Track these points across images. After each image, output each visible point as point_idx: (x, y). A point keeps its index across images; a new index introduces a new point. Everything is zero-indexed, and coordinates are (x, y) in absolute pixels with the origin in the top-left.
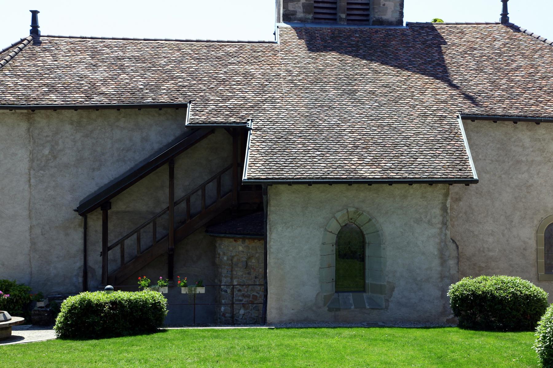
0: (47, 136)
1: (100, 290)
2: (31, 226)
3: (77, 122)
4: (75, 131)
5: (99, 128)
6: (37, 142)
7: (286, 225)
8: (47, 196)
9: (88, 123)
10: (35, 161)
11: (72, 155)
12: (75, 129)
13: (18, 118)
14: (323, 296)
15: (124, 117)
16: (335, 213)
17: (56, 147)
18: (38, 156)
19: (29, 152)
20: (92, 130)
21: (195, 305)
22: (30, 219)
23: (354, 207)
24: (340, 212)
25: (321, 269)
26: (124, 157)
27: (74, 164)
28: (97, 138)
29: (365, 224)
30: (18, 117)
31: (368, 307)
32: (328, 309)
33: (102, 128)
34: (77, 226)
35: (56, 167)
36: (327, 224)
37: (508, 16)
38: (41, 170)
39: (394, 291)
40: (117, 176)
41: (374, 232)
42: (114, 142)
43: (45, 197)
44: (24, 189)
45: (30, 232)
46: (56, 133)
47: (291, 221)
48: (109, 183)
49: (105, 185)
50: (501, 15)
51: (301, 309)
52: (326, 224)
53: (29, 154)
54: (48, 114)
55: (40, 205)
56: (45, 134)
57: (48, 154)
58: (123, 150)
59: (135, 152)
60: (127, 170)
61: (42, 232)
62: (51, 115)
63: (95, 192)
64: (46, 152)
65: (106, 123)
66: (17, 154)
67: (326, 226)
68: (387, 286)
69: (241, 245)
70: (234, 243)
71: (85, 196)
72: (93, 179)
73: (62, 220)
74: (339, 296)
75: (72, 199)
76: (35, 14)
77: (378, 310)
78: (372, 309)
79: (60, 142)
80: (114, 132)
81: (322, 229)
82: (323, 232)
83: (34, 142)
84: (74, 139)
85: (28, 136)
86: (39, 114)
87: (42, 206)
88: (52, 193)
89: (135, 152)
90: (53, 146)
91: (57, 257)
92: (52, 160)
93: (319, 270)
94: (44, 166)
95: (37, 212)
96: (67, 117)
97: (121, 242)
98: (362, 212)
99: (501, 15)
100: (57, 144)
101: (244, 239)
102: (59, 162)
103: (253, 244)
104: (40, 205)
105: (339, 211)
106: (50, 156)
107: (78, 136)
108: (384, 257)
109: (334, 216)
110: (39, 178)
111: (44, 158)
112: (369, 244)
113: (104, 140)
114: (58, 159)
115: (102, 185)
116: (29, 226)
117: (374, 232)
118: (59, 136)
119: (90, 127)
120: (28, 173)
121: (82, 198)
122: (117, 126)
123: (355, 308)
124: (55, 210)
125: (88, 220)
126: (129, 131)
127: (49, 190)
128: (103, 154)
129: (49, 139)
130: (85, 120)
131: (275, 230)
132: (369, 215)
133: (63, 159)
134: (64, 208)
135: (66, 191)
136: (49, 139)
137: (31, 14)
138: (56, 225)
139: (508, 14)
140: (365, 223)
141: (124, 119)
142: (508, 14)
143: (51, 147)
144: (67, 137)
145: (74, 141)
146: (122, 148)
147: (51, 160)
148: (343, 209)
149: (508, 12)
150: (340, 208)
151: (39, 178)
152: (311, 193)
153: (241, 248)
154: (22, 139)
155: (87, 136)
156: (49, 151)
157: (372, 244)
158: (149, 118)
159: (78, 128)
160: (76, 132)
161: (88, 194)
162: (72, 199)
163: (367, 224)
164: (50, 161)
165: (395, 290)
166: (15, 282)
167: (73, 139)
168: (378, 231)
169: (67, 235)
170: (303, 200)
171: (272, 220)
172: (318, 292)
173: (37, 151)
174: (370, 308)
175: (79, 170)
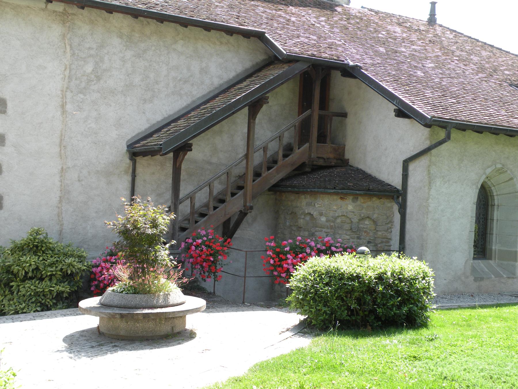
0: (90, 48)
2: (62, 168)
3: (128, 36)
4: (125, 48)
5: (153, 48)
6: (77, 54)
7: (444, 180)
8: (86, 130)
9: (141, 39)
10: (74, 80)
11: (120, 79)
12: (125, 45)
13: (50, 18)
15: (182, 39)
16: (486, 169)
17: (101, 65)
18: (77, 73)
19: (64, 67)
20: (145, 50)
21: (246, 276)
22: (61, 158)
23: (501, 164)
25: (470, 232)
26: (181, 90)
27: (122, 91)
28: (151, 61)
30: (49, 16)
31: (505, 276)
33: (157, 50)
34: (123, 172)
35: (98, 92)
37: (436, 16)
38: (80, 93)
40: (171, 113)
41: (510, 193)
42: (170, 69)
43: (85, 130)
44: (53, 117)
45: (61, 176)
46: (101, 46)
47: (448, 175)
48: (162, 120)
49: (158, 122)
50: (429, 15)
51: (452, 279)
52: (478, 181)
53: (64, 69)
54: (93, 18)
55: (78, 141)
56: (88, 46)
57: (91, 73)
58: (180, 80)
59: (192, 85)
60: (183, 106)
61: (79, 177)
62: (96, 20)
63: (146, 130)
64: (89, 68)
65: (161, 43)
66: (45, 68)
69: (351, 204)
70: (339, 202)
71: (134, 135)
72: (144, 113)
73: (105, 163)
75: (117, 137)
76: (433, 4)
78: (509, 278)
79: (106, 58)
80: (170, 56)
81: (474, 187)
82: (475, 190)
83: (73, 54)
84: (123, 57)
85: (63, 45)
86: (81, 16)
87: (80, 142)
88: (93, 125)
89: (192, 85)
90: (97, 63)
91: (96, 212)
92: (95, 81)
93: (469, 234)
94: (85, 88)
95: (73, 150)
96: (115, 27)
97: (191, 197)
98: (506, 169)
99: (429, 15)
100: (102, 60)
101: (356, 198)
102: (103, 86)
103: (370, 203)
104: (78, 141)
105: (489, 167)
106: (93, 76)
107: (129, 54)
110: (77, 104)
111: (86, 78)
112: (498, 206)
113: (159, 65)
114: (102, 82)
115: (154, 122)
116: (60, 168)
118: (106, 51)
119: (142, 45)
120: (61, 96)
121: (129, 137)
122: (175, 50)
124: (96, 149)
125: (138, 165)
126: (188, 57)
127: (89, 122)
128: (157, 83)
129: (92, 52)
130: (137, 35)
131: (434, 185)
133: (108, 82)
134: (107, 147)
135: (111, 125)
136: (92, 52)
137: (430, 5)
138: (97, 169)
139: (436, 15)
140: (500, 183)
141: (181, 42)
142: (436, 15)
143: (95, 63)
144: (114, 54)
145: (123, 60)
146: (179, 78)
147: (93, 81)
149: (436, 14)
150: (490, 164)
151: (77, 104)
152: (467, 144)
153: (350, 207)
154: (54, 47)
155: (139, 56)
156: (92, 68)
158: (210, 46)
159: (128, 43)
160: (126, 49)
161: (136, 132)
162: (117, 137)
163: (503, 184)
164: (93, 83)
167: (122, 57)
169: (109, 183)
170: (459, 151)
171: (432, 172)
172: (466, 259)
173: (77, 67)
174: (507, 277)
175: (128, 100)
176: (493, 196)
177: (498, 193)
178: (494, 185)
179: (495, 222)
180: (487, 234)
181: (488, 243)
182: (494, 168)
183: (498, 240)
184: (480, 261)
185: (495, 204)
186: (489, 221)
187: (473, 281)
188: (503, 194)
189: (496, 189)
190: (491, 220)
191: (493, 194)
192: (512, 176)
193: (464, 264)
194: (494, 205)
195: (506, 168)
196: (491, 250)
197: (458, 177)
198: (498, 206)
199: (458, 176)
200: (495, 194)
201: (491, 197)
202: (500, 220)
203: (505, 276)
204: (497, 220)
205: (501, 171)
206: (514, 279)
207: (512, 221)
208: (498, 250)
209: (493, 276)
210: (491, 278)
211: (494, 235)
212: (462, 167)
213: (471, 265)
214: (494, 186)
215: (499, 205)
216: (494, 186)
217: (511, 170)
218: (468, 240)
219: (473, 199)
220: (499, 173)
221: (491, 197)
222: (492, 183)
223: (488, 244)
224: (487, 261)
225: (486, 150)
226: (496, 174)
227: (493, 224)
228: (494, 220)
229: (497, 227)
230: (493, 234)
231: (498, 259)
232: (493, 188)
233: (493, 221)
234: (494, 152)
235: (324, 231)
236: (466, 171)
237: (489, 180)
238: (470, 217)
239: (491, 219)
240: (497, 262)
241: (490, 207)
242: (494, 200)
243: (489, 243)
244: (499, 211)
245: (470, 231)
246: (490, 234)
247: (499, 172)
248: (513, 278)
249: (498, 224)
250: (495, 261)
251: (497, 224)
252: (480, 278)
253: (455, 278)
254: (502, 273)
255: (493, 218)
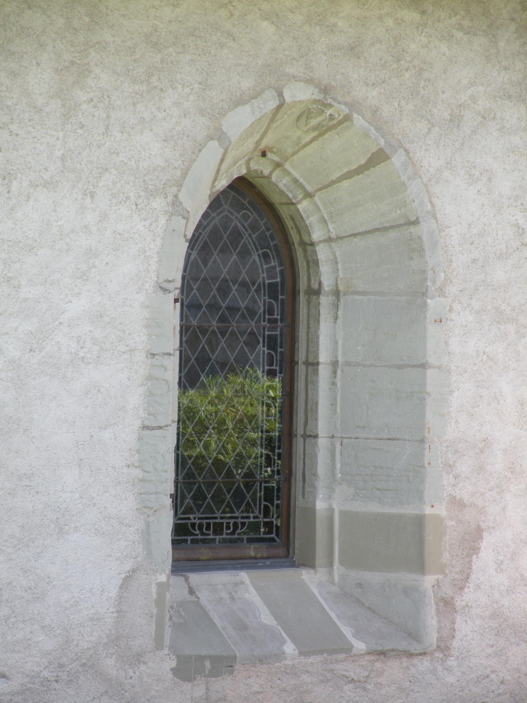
1: (351, 170)
14: (154, 589)
16: (223, 114)
23: (309, 81)
24: (248, 107)
29: (333, 183)
31: (360, 646)
32: (174, 664)
36: (185, 173)
39: (475, 550)
41: (385, 229)
51: (45, 674)
52: (179, 173)
67: (180, 185)
68: (450, 523)
74: (191, 592)
77: (405, 661)
82: (163, 221)
93: (140, 439)
98: (346, 110)
105: (239, 102)
108: (440, 367)
109: (219, 129)
112: (337, 293)
117: (385, 229)
123: (301, 654)
132: (378, 129)
140: (334, 177)
148: (262, 91)
157: (364, 293)
163: (346, 183)
165: (484, 544)
166: (318, 447)
168: (416, 222)
172: (128, 566)
176: (312, 244)
177: (333, 230)
178: (309, 188)
179: (324, 372)
180: (296, 436)
181: (300, 483)
182: (273, 104)
183: (338, 466)
184: (244, 576)
185: (320, 284)
186: (301, 369)
187: (170, 675)
188: (355, 235)
189: (319, 210)
190: (310, 368)
191: (309, 235)
192: (382, 142)
193: (114, 592)
194: (318, 293)
195: (346, 104)
196: (311, 512)
197: (63, 159)
198: (337, 293)
199: (59, 154)
200: (317, 235)
201: (305, 251)
202: (348, 364)
203: (360, 646)
204: (335, 364)
205: (319, 119)
206: (416, 661)
207: (400, 367)
208: (344, 514)
209: (290, 648)
210: (280, 656)
211: (322, 442)
212: (84, 107)
213: (155, 596)
214: (309, 195)
215: (341, 288)
216: (309, 195)
217: (375, 111)
218: (138, 473)
219: (154, 267)
220: (314, 129)
221: (305, 251)
222: (296, 181)
223: (299, 489)
224: (289, 573)
225: (223, 12)
226: (299, 133)
227: (315, 383)
228: (318, 364)
229: (334, 404)
230: (316, 436)
231: (342, 563)
232: (303, 206)
233: (316, 372)
234: (265, 24)
235: (201, 231)
236: (107, 127)
237: (278, 165)
238: (140, 357)
239: (307, 363)
240: (336, 579)
241: (302, 299)
242: (316, 263)
243: (304, 481)
244: (340, 321)
245: (145, 427)
246: (305, 436)
247: (314, 122)
248: (410, 655)
249: (339, 385)
250: (331, 573)
251: (334, 384)
252: (215, 660)
253: (61, 666)
254: (347, 632)
255: (317, 356)
